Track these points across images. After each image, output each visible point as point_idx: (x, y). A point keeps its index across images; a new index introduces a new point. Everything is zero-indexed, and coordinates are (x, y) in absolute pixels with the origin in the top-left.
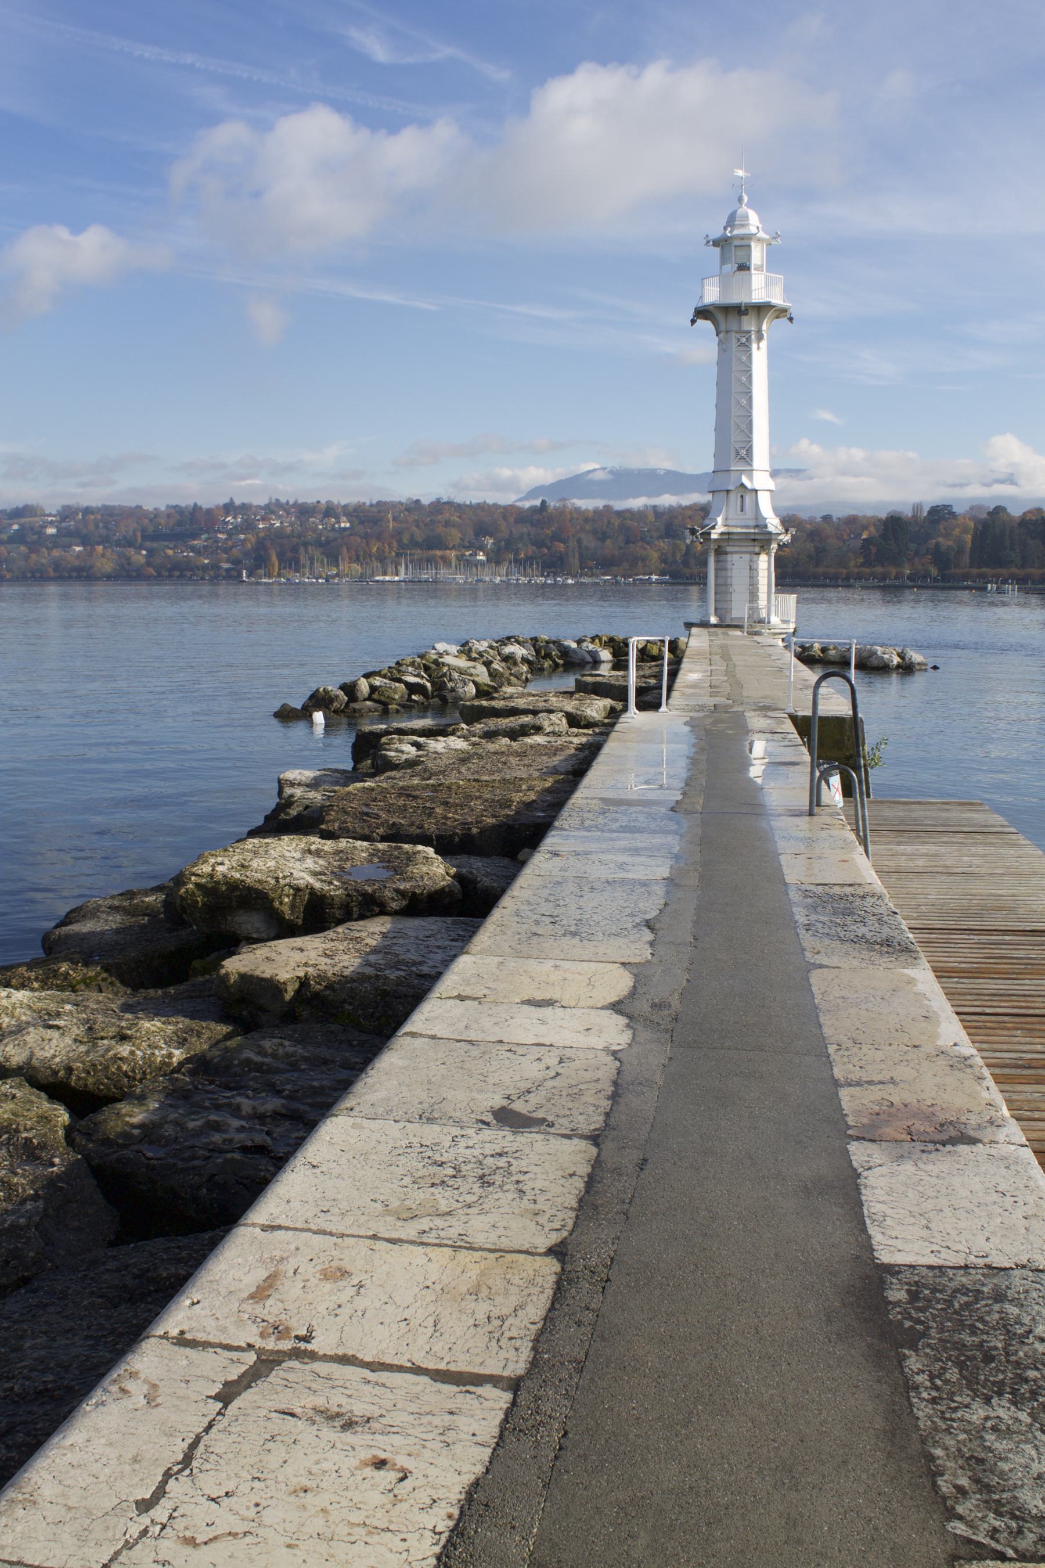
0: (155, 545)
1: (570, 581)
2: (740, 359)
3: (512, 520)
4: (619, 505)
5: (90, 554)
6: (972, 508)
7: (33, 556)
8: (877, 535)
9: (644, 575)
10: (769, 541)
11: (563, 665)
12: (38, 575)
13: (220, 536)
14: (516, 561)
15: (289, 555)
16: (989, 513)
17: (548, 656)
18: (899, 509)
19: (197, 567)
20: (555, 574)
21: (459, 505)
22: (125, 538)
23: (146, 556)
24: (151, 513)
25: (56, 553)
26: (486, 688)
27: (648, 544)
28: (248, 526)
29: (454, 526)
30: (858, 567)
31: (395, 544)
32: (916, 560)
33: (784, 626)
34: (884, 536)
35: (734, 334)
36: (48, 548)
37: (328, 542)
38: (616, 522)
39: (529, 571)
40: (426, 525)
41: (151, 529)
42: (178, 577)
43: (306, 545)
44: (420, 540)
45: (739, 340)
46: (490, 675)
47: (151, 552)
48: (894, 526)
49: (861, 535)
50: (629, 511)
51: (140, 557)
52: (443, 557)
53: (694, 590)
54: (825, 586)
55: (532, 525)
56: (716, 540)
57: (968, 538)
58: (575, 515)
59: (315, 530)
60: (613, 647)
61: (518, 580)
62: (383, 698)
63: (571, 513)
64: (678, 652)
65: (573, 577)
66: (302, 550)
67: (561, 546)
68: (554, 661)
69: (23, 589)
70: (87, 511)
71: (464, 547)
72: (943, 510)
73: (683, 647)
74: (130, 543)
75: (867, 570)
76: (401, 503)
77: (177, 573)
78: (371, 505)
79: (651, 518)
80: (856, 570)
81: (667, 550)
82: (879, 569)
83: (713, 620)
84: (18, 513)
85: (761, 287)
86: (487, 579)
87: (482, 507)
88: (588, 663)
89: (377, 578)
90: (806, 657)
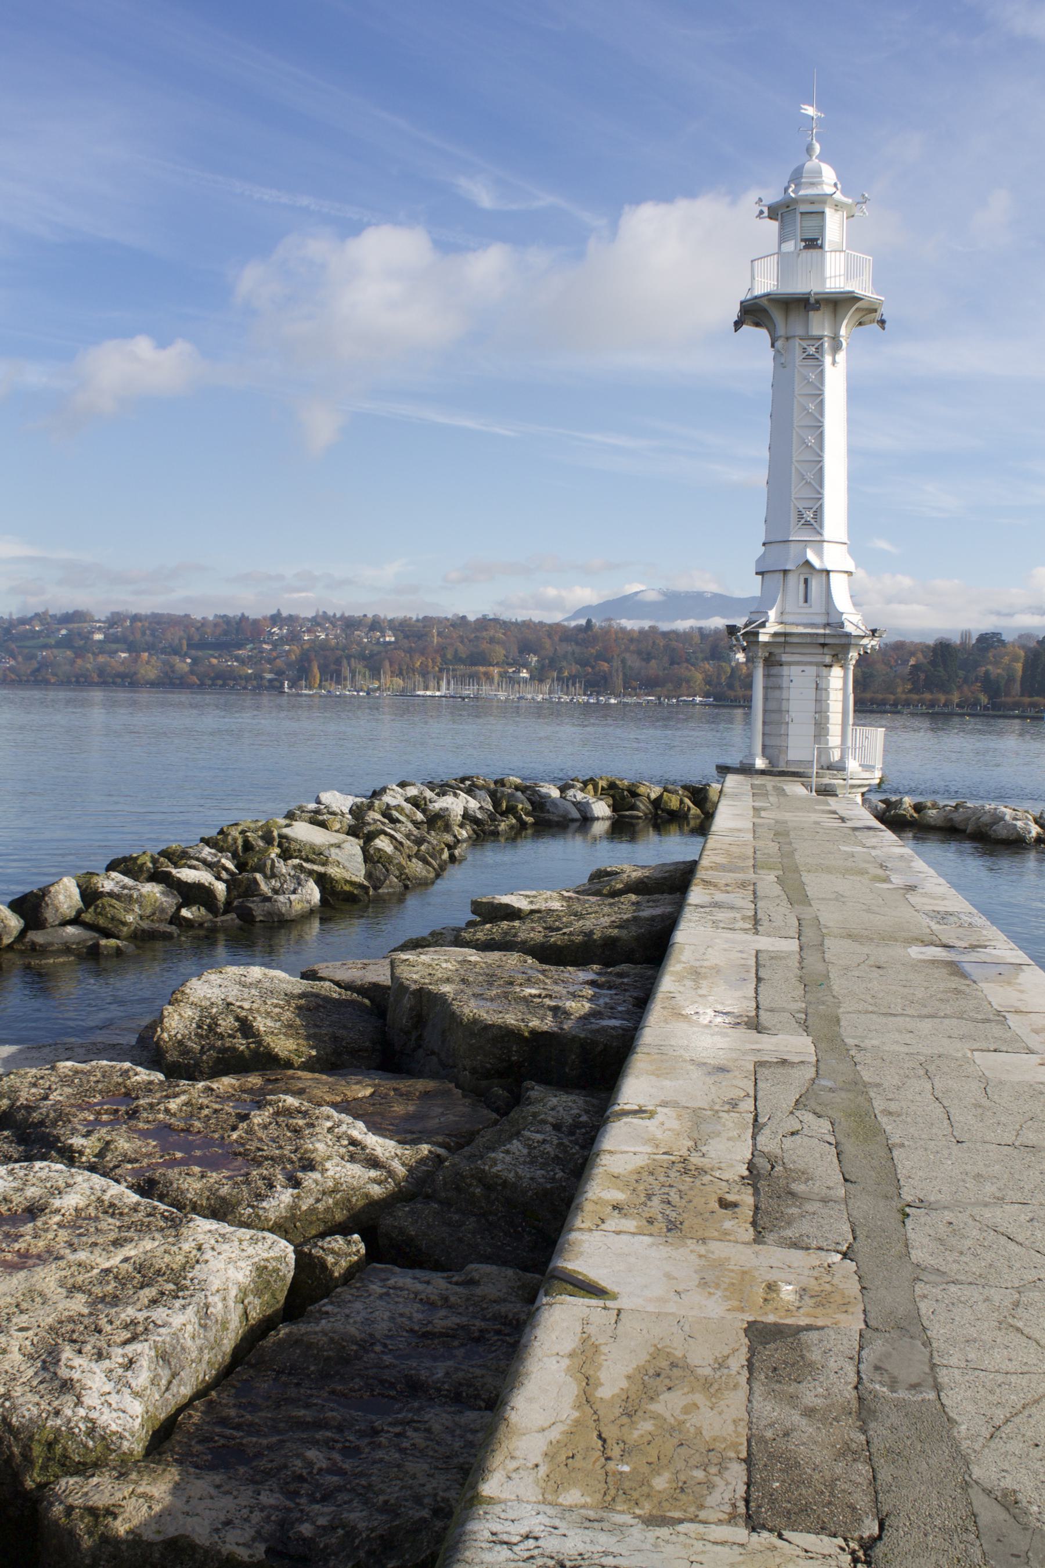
0: (200, 653)
1: (613, 701)
2: (805, 378)
3: (556, 638)
4: (665, 626)
5: (135, 661)
6: (1020, 637)
7: (79, 661)
8: (925, 661)
9: (688, 696)
10: (845, 647)
11: (534, 824)
12: (82, 680)
13: (265, 646)
14: (559, 679)
15: (333, 667)
16: (1038, 642)
17: (511, 810)
18: (947, 636)
19: (240, 677)
20: (599, 694)
21: (505, 622)
22: (171, 646)
23: (190, 665)
24: (199, 622)
25: (101, 659)
26: (347, 888)
28: (293, 637)
29: (498, 643)
31: (439, 659)
32: (965, 688)
33: (867, 775)
34: (933, 663)
35: (797, 341)
36: (94, 654)
37: (372, 656)
38: (662, 643)
40: (470, 641)
41: (197, 637)
42: (210, 686)
43: (349, 657)
44: (464, 656)
45: (804, 350)
46: (367, 858)
47: (195, 661)
48: (943, 652)
49: (908, 661)
50: (674, 632)
51: (183, 665)
52: (486, 674)
53: (739, 712)
54: (872, 712)
55: (577, 644)
56: (766, 644)
57: (1019, 666)
58: (620, 635)
59: (359, 643)
60: (613, 797)
61: (559, 698)
62: (101, 921)
63: (616, 633)
64: (708, 805)
65: (616, 696)
66: (345, 662)
67: (605, 666)
68: (519, 819)
69: (71, 694)
70: (135, 618)
71: (508, 664)
72: (992, 638)
73: (715, 799)
74: (176, 652)
75: (915, 697)
76: (447, 619)
77: (220, 682)
78: (418, 620)
79: (697, 639)
80: (904, 696)
81: (709, 671)
82: (928, 696)
83: (760, 763)
84: (68, 618)
85: (836, 273)
86: (529, 696)
87: (527, 625)
88: (573, 820)
89: (419, 693)
90: (893, 819)
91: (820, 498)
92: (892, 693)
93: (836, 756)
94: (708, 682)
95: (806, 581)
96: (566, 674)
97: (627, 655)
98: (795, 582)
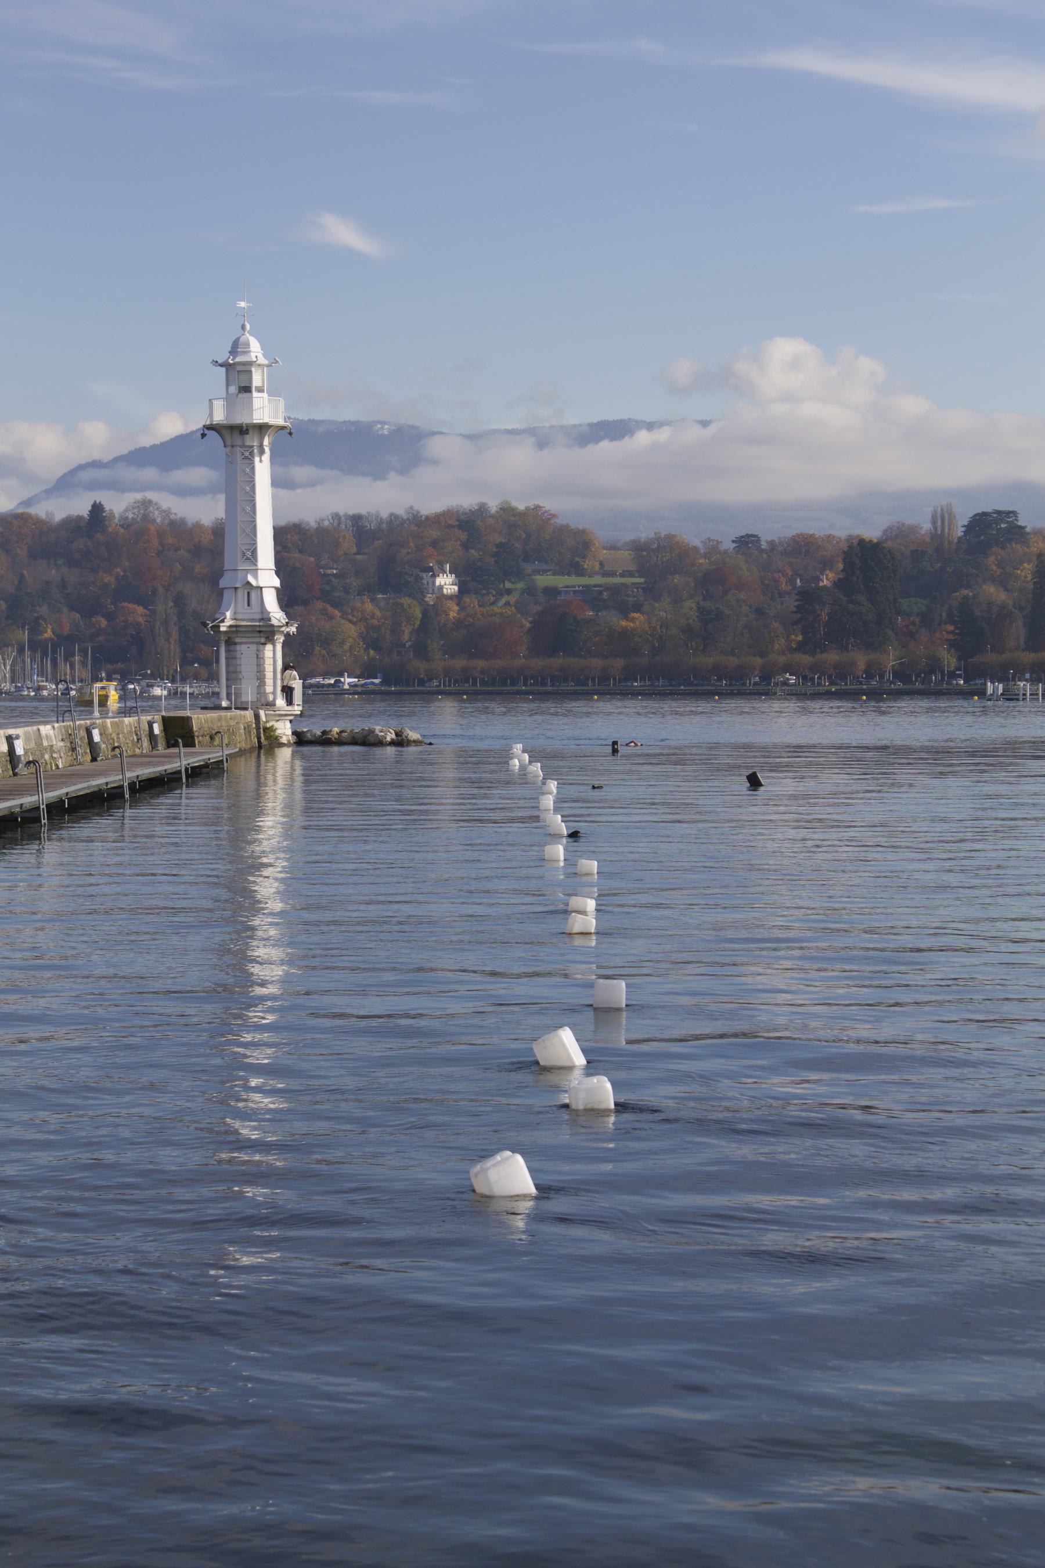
2: (244, 471)
3: (22, 552)
9: (325, 675)
14: (34, 646)
27: (335, 605)
30: (792, 651)
39: (65, 668)
48: (866, 560)
56: (225, 632)
58: (170, 540)
61: (39, 689)
75: (806, 659)
79: (349, 545)
82: (833, 657)
83: (224, 704)
85: (264, 409)
91: (255, 544)
92: (762, 655)
93: (271, 698)
94: (372, 641)
95: (248, 593)
96: (49, 634)
97: (187, 587)
98: (242, 595)
